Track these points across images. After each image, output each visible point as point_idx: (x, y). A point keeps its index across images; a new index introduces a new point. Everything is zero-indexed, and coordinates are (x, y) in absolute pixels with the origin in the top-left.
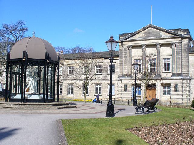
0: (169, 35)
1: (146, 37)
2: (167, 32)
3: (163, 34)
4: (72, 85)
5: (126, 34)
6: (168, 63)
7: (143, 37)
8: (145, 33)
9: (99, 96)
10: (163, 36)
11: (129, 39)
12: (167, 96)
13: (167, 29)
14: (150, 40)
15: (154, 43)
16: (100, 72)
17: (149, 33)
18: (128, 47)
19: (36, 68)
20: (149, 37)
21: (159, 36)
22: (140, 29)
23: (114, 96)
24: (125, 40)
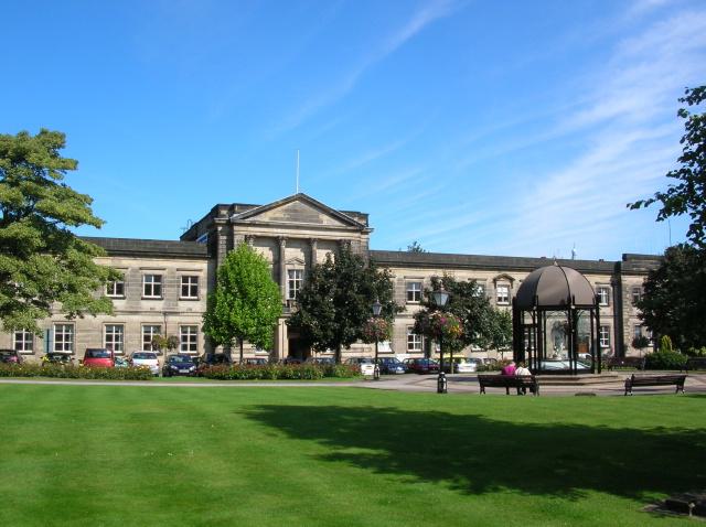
0: (337, 223)
1: (288, 219)
2: (334, 215)
3: (326, 220)
4: (158, 278)
5: (247, 206)
6: (187, 295)
7: (282, 219)
8: (286, 210)
9: (113, 301)
10: (325, 223)
11: (251, 219)
12: (414, 350)
13: (336, 206)
14: (298, 227)
15: (307, 237)
16: (157, 293)
17: (296, 211)
18: (247, 238)
19: (193, 347)
20: (296, 220)
21: (317, 222)
22: (279, 199)
23: (508, 393)
24: (242, 221)
